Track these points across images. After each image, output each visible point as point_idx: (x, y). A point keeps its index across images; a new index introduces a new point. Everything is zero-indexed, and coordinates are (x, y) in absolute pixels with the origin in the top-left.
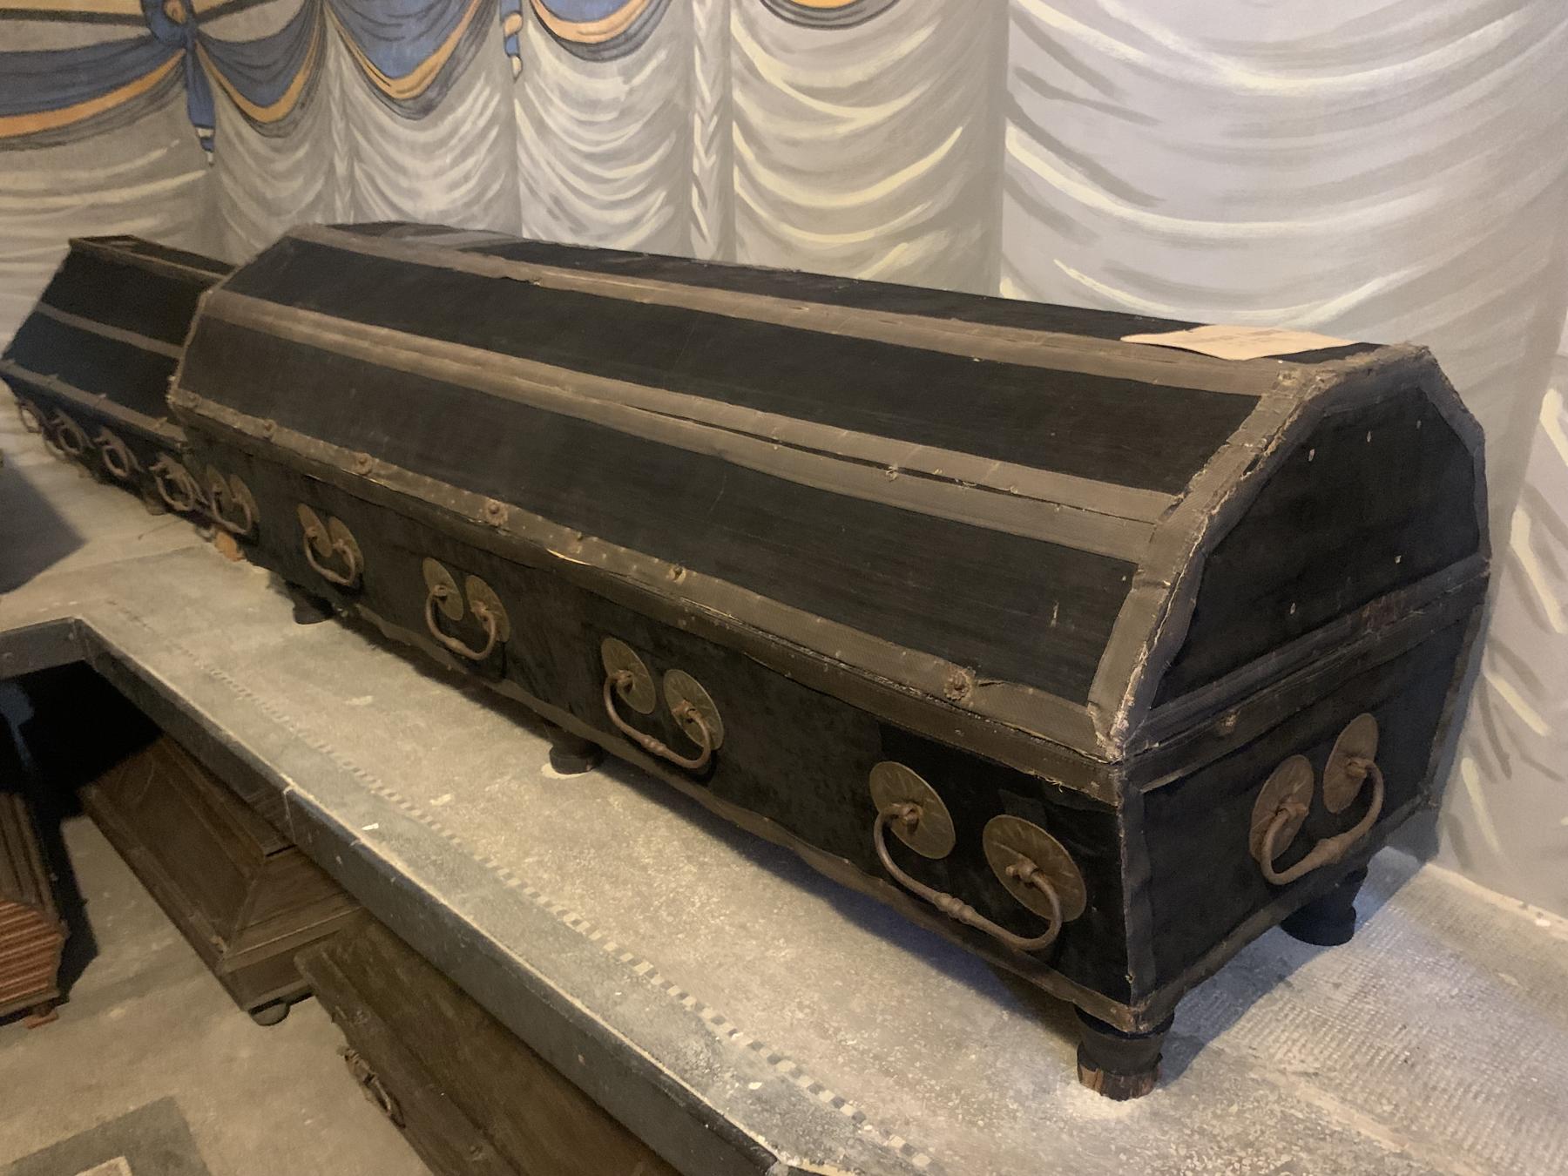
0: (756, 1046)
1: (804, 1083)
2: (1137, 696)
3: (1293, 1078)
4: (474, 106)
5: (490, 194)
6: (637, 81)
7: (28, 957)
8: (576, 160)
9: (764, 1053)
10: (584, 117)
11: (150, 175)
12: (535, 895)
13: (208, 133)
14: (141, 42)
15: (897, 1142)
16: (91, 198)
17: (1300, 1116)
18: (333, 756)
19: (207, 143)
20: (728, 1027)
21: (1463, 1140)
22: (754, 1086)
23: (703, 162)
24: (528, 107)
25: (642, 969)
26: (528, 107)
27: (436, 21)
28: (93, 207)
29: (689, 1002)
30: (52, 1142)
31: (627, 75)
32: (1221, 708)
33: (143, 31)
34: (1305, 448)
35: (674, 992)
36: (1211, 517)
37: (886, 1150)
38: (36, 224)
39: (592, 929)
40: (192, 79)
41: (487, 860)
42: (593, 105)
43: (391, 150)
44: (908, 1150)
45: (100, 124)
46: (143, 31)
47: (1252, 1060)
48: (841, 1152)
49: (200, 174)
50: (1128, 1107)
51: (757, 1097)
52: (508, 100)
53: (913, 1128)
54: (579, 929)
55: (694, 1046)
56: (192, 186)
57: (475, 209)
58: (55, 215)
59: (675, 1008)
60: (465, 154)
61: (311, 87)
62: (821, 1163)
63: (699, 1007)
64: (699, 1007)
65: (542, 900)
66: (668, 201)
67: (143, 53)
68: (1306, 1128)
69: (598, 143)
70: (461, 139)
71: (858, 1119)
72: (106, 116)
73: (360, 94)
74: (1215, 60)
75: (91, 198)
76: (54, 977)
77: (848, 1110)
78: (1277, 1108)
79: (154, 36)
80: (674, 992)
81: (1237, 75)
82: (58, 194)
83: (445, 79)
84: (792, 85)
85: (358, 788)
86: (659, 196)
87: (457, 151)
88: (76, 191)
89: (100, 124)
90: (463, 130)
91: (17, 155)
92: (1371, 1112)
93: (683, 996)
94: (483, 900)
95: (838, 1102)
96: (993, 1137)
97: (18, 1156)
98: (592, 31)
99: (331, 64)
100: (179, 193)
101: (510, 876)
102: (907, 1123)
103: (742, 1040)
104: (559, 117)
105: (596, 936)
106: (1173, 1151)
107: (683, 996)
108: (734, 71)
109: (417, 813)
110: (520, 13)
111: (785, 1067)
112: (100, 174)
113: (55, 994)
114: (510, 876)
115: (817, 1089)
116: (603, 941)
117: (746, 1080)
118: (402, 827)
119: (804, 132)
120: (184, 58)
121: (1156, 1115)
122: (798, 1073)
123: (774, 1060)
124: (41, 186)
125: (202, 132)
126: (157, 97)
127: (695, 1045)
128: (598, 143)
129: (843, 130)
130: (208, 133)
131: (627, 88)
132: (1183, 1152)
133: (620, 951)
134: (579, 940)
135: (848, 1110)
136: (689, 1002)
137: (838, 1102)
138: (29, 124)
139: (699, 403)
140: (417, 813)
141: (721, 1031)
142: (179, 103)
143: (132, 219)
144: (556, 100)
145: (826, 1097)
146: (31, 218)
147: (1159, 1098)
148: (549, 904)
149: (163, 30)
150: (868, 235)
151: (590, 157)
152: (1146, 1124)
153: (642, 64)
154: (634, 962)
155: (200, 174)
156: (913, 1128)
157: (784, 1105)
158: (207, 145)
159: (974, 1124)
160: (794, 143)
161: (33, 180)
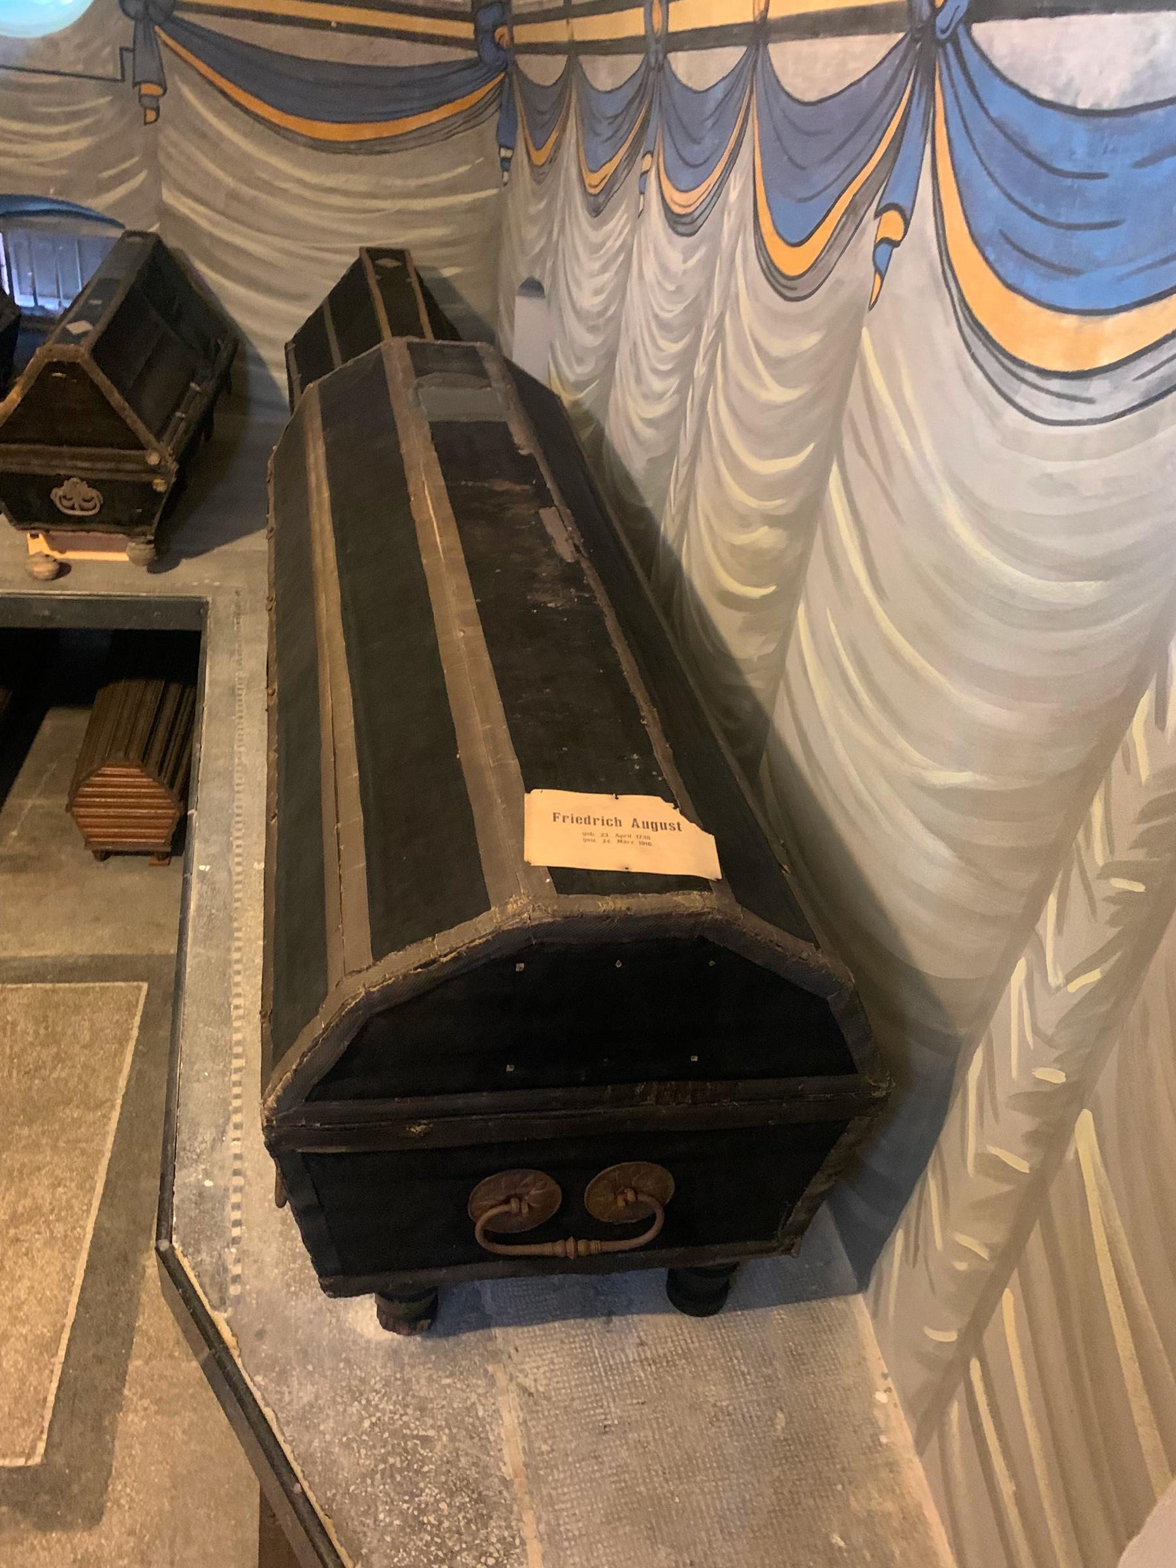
0: (237, 1157)
1: (235, 1198)
2: (284, 1090)
3: (513, 1387)
4: (618, 222)
5: (610, 313)
6: (691, 263)
7: (153, 818)
8: (650, 313)
9: (237, 1165)
10: (660, 278)
11: (452, 188)
12: (239, 973)
13: (508, 154)
14: (470, 64)
15: (237, 1270)
16: (401, 204)
17: (480, 1414)
18: (237, 796)
19: (506, 161)
20: (238, 1134)
21: (563, 1502)
22: (208, 1183)
23: (700, 369)
24: (639, 244)
25: (237, 1063)
26: (639, 244)
27: (617, 131)
28: (400, 212)
29: (236, 1103)
30: (118, 952)
31: (687, 255)
32: (414, 1118)
33: (472, 54)
34: (513, 959)
35: (236, 1090)
36: (368, 993)
37: (226, 1270)
38: (353, 222)
39: (239, 1018)
40: (503, 99)
41: (239, 930)
42: (664, 269)
43: (576, 234)
44: (236, 1279)
45: (423, 136)
46: (472, 54)
47: (505, 1357)
48: (204, 1255)
49: (493, 192)
50: (388, 1335)
51: (202, 1194)
52: (633, 232)
53: (255, 1267)
54: (234, 1013)
55: (207, 1135)
56: (485, 201)
57: (601, 321)
58: (368, 215)
59: (226, 1102)
60: (604, 269)
61: (558, 146)
62: (185, 1256)
63: (237, 1110)
64: (237, 1110)
65: (237, 979)
66: (677, 391)
67: (468, 75)
68: (473, 1425)
69: (662, 309)
70: (606, 252)
71: (235, 1241)
72: (428, 130)
73: (574, 171)
74: (946, 489)
75: (401, 204)
76: (170, 838)
77: (236, 1232)
78: (474, 1397)
79: (480, 60)
80: (236, 1090)
81: (952, 512)
82: (374, 196)
83: (609, 188)
84: (751, 331)
85: (228, 832)
86: (674, 382)
87: (603, 261)
88: (385, 198)
89: (423, 136)
90: (609, 244)
91: (352, 159)
92: (530, 1442)
93: (237, 1097)
94: (209, 960)
95: (237, 1223)
96: (287, 1302)
97: (96, 952)
98: (680, 201)
99: (568, 132)
100: (472, 208)
101: (239, 949)
102: (255, 1261)
103: (236, 1148)
104: (650, 269)
105: (236, 1024)
106: (373, 1382)
107: (237, 1097)
108: (730, 299)
109: (239, 869)
110: (652, 153)
111: (238, 1181)
112: (413, 183)
113: (169, 849)
114: (239, 949)
115: (237, 1207)
116: (237, 1030)
117: (207, 1175)
118: (222, 876)
119: (748, 384)
120: (502, 81)
121: (394, 1354)
122: (238, 1189)
123: (236, 1173)
124: (363, 188)
125: (504, 153)
126: (472, 117)
127: (208, 1135)
128: (662, 309)
129: (765, 396)
130: (508, 154)
131: (683, 267)
132: (377, 1387)
133: (238, 1043)
134: (227, 1020)
135: (236, 1232)
136: (236, 1103)
137: (237, 1223)
138: (367, 132)
139: (346, 689)
140: (239, 869)
141: (232, 1133)
142: (490, 125)
143: (428, 227)
144: (651, 249)
145: (236, 1215)
146: (346, 215)
147: (413, 1343)
148: (237, 984)
149: (489, 54)
150: (753, 503)
151: (656, 316)
152: (381, 1354)
153: (695, 248)
154: (237, 1056)
155: (493, 192)
156: (255, 1267)
157: (209, 1206)
158: (506, 165)
159: (289, 1286)
160: (741, 388)
161: (359, 182)
